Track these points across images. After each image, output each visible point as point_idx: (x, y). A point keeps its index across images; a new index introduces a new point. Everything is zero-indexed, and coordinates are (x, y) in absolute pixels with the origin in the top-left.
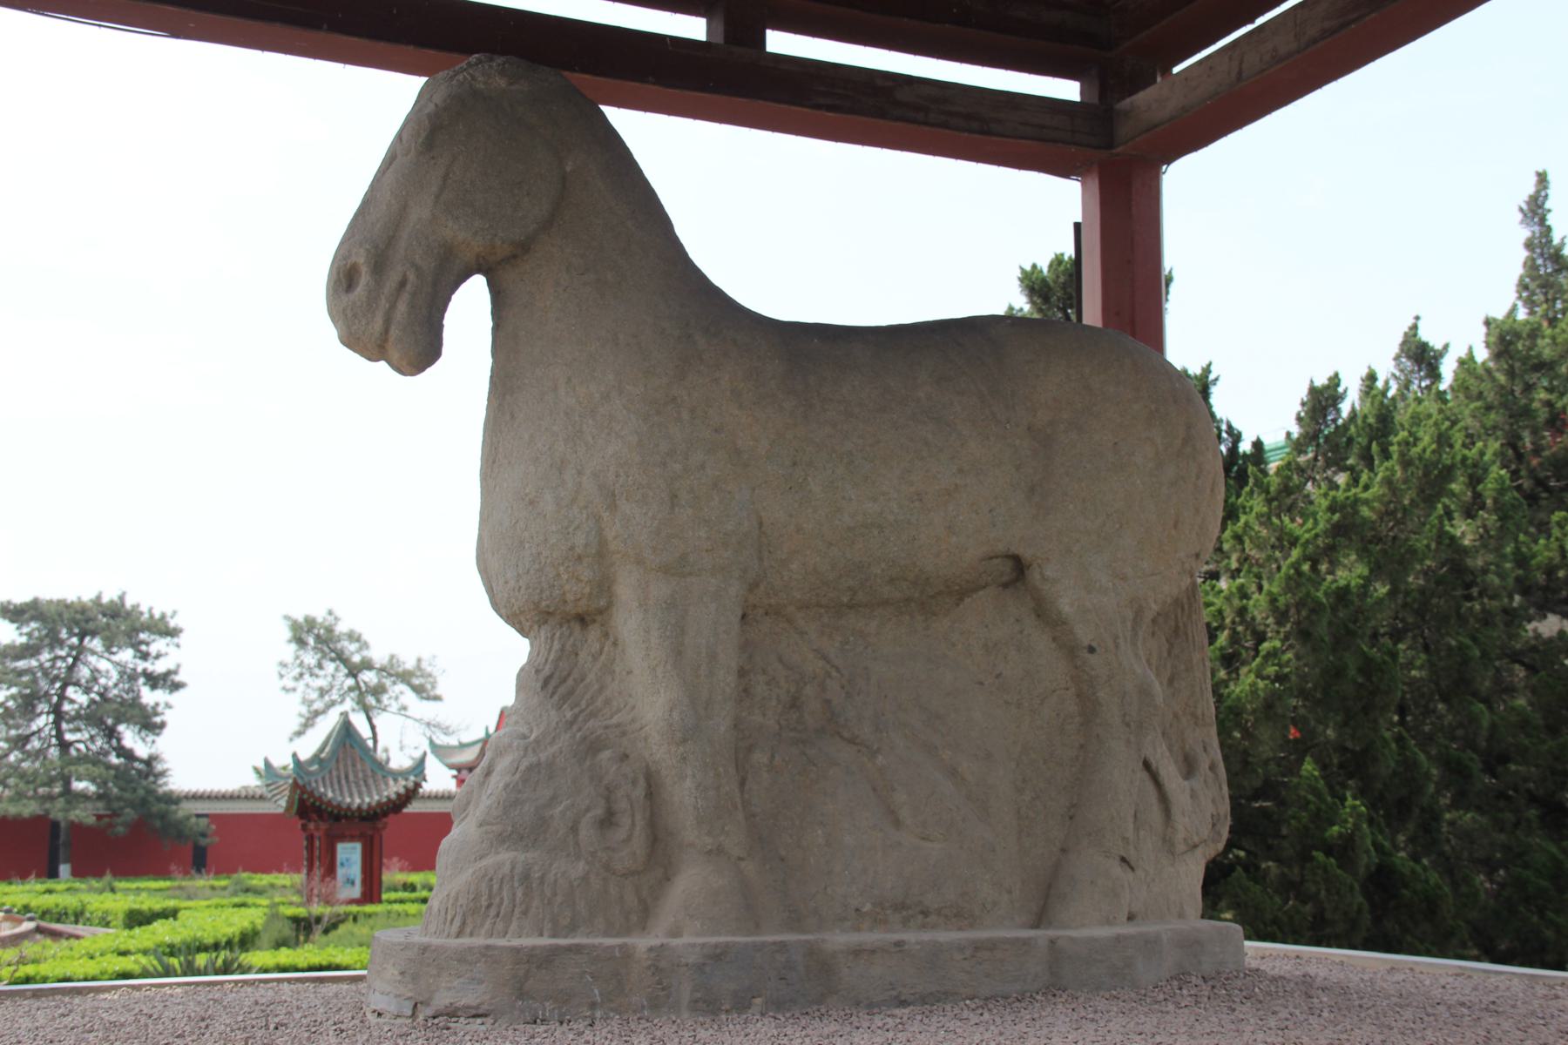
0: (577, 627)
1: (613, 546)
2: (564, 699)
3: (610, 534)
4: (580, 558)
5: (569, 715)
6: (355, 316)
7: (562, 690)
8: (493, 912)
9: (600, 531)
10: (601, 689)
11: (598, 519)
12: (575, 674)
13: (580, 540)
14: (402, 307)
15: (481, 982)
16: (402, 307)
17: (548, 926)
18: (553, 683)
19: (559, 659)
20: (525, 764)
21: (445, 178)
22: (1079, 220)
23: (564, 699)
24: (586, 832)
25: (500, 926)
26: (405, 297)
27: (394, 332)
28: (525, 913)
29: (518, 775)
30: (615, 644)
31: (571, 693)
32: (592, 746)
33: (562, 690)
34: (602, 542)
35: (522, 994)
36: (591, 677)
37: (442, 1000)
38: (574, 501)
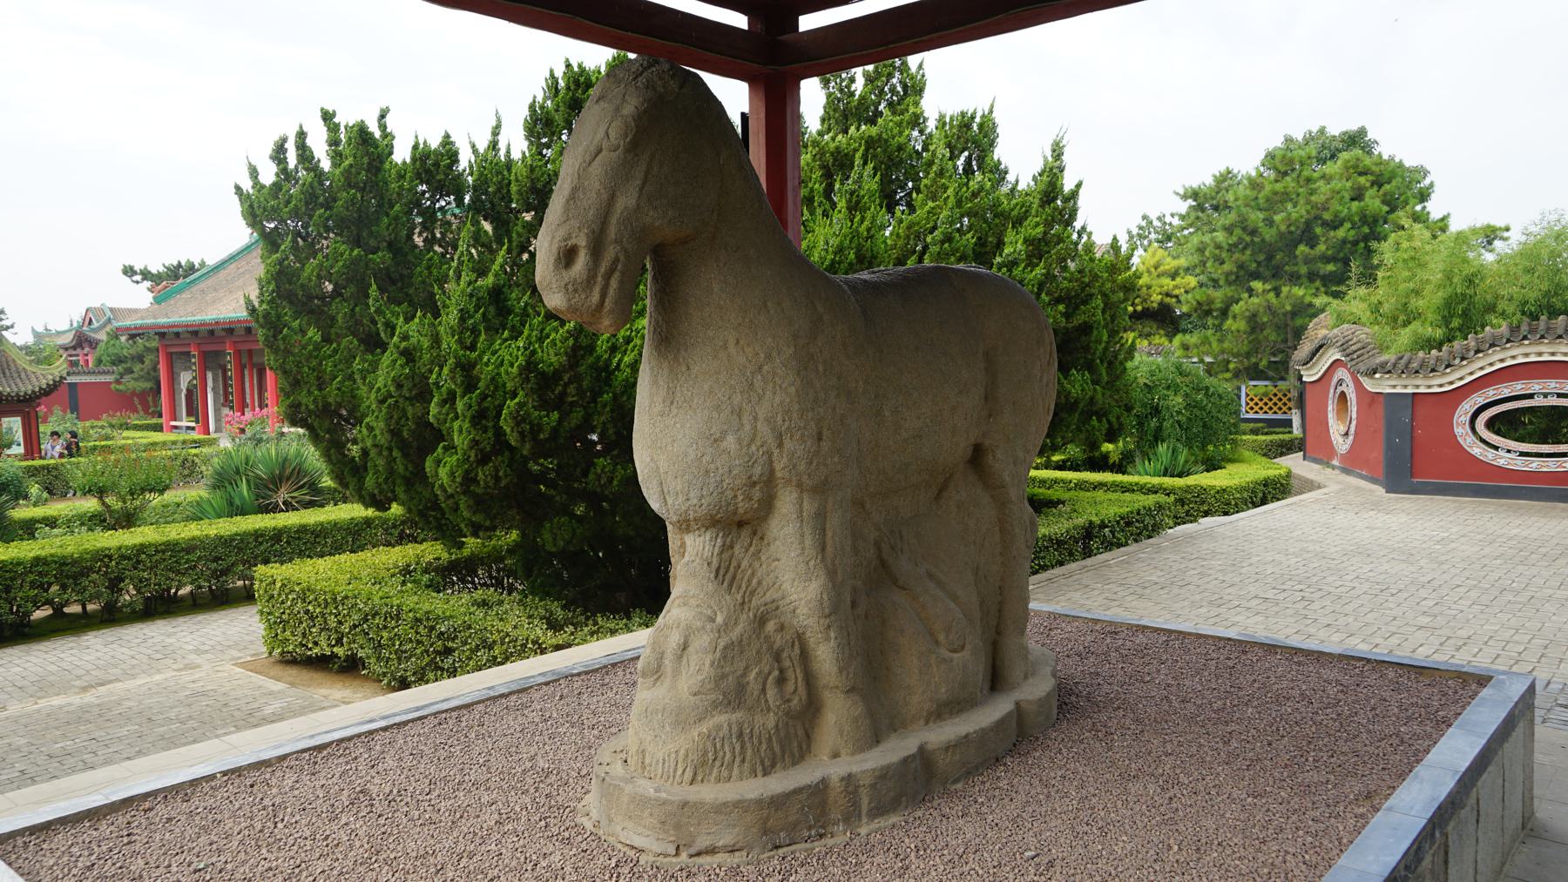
0: (735, 529)
1: (779, 475)
2: (731, 585)
3: (778, 466)
4: (755, 484)
5: (739, 597)
6: (576, 291)
7: (729, 576)
8: (718, 763)
9: (771, 462)
10: (753, 574)
11: (770, 455)
12: (734, 563)
13: (758, 470)
14: (614, 284)
15: (734, 826)
16: (614, 284)
17: (759, 769)
18: (722, 572)
19: (722, 553)
20: (722, 644)
21: (647, 173)
22: (746, 110)
23: (731, 585)
24: (771, 693)
25: (725, 774)
26: (617, 275)
27: (608, 303)
28: (743, 761)
29: (718, 654)
30: (762, 538)
31: (734, 578)
32: (761, 621)
33: (729, 576)
34: (772, 471)
35: (765, 832)
36: (745, 564)
37: (703, 842)
38: (753, 440)
